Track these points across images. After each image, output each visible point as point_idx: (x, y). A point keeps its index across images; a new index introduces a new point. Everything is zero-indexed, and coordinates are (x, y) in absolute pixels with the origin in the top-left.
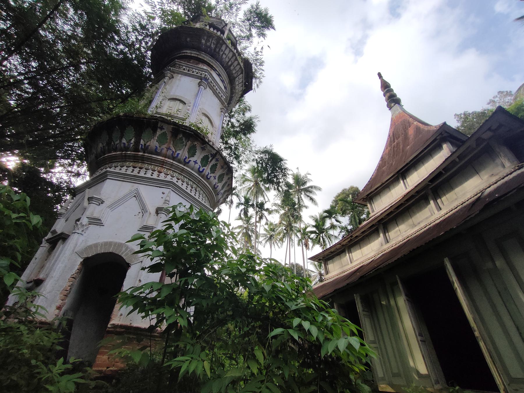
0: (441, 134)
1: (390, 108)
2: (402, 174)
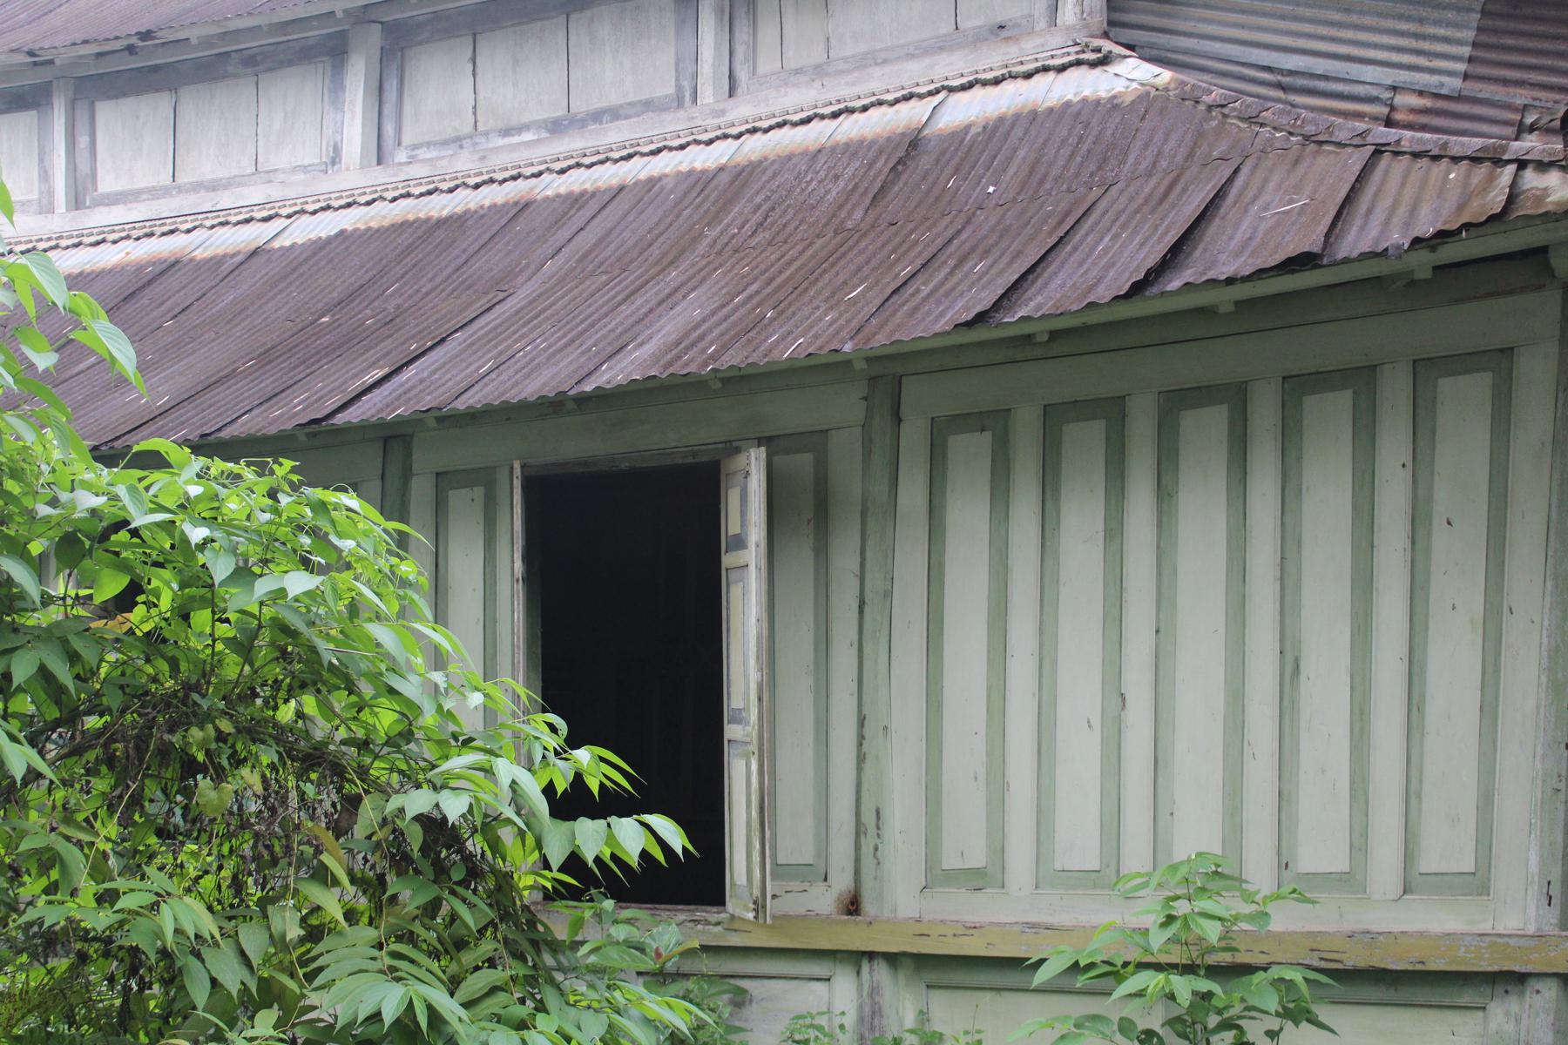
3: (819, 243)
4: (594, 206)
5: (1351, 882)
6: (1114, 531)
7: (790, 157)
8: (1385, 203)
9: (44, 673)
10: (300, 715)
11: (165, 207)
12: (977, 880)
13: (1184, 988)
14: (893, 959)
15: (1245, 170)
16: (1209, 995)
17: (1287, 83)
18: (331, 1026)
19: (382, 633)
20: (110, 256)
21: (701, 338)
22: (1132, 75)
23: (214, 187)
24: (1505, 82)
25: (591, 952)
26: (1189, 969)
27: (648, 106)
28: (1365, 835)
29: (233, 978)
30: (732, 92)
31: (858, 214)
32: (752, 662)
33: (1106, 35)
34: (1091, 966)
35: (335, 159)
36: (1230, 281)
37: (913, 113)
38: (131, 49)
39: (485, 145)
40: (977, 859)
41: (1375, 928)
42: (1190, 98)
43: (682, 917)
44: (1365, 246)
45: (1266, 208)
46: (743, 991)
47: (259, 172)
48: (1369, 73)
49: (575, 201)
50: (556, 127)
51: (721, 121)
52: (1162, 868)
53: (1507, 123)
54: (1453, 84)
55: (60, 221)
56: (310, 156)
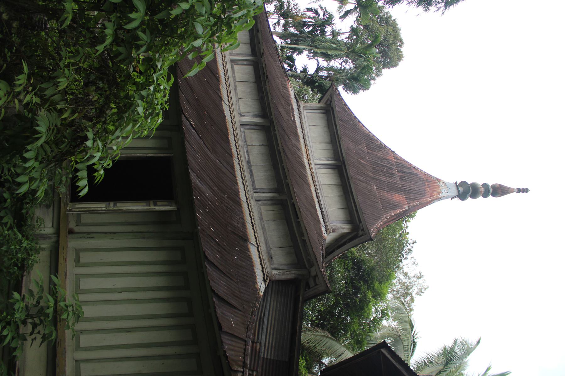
0: (363, 230)
1: (457, 186)
2: (340, 167)
3: (223, 221)
4: (231, 171)
5: (78, 348)
6: (159, 289)
7: (243, 213)
8: (233, 343)
9: (121, 54)
10: (112, 108)
11: (231, 79)
12: (77, 261)
13: (50, 311)
14: (58, 242)
15: (241, 313)
16: (49, 317)
17: (261, 321)
18: (36, 115)
19: (129, 127)
20: (220, 67)
21: (201, 195)
22: (262, 287)
23: (235, 89)
24: (262, 366)
25: (59, 172)
26: (55, 311)
27: (253, 182)
28: (89, 350)
29: (48, 93)
30: (256, 200)
31: (230, 229)
32: (128, 208)
33: (270, 280)
34: (56, 289)
35: (241, 115)
36: (215, 312)
37: (253, 240)
38: (264, 73)
39: (245, 147)
40: (82, 260)
41: (66, 354)
42: (257, 299)
43: (68, 193)
44: (224, 340)
45: (232, 318)
46: (50, 207)
47: (238, 99)
48: (264, 337)
49: (233, 167)
50: (249, 162)
51: (250, 198)
52: (80, 304)
53: (254, 368)
54: (262, 355)
55: (228, 57)
56: (242, 110)
